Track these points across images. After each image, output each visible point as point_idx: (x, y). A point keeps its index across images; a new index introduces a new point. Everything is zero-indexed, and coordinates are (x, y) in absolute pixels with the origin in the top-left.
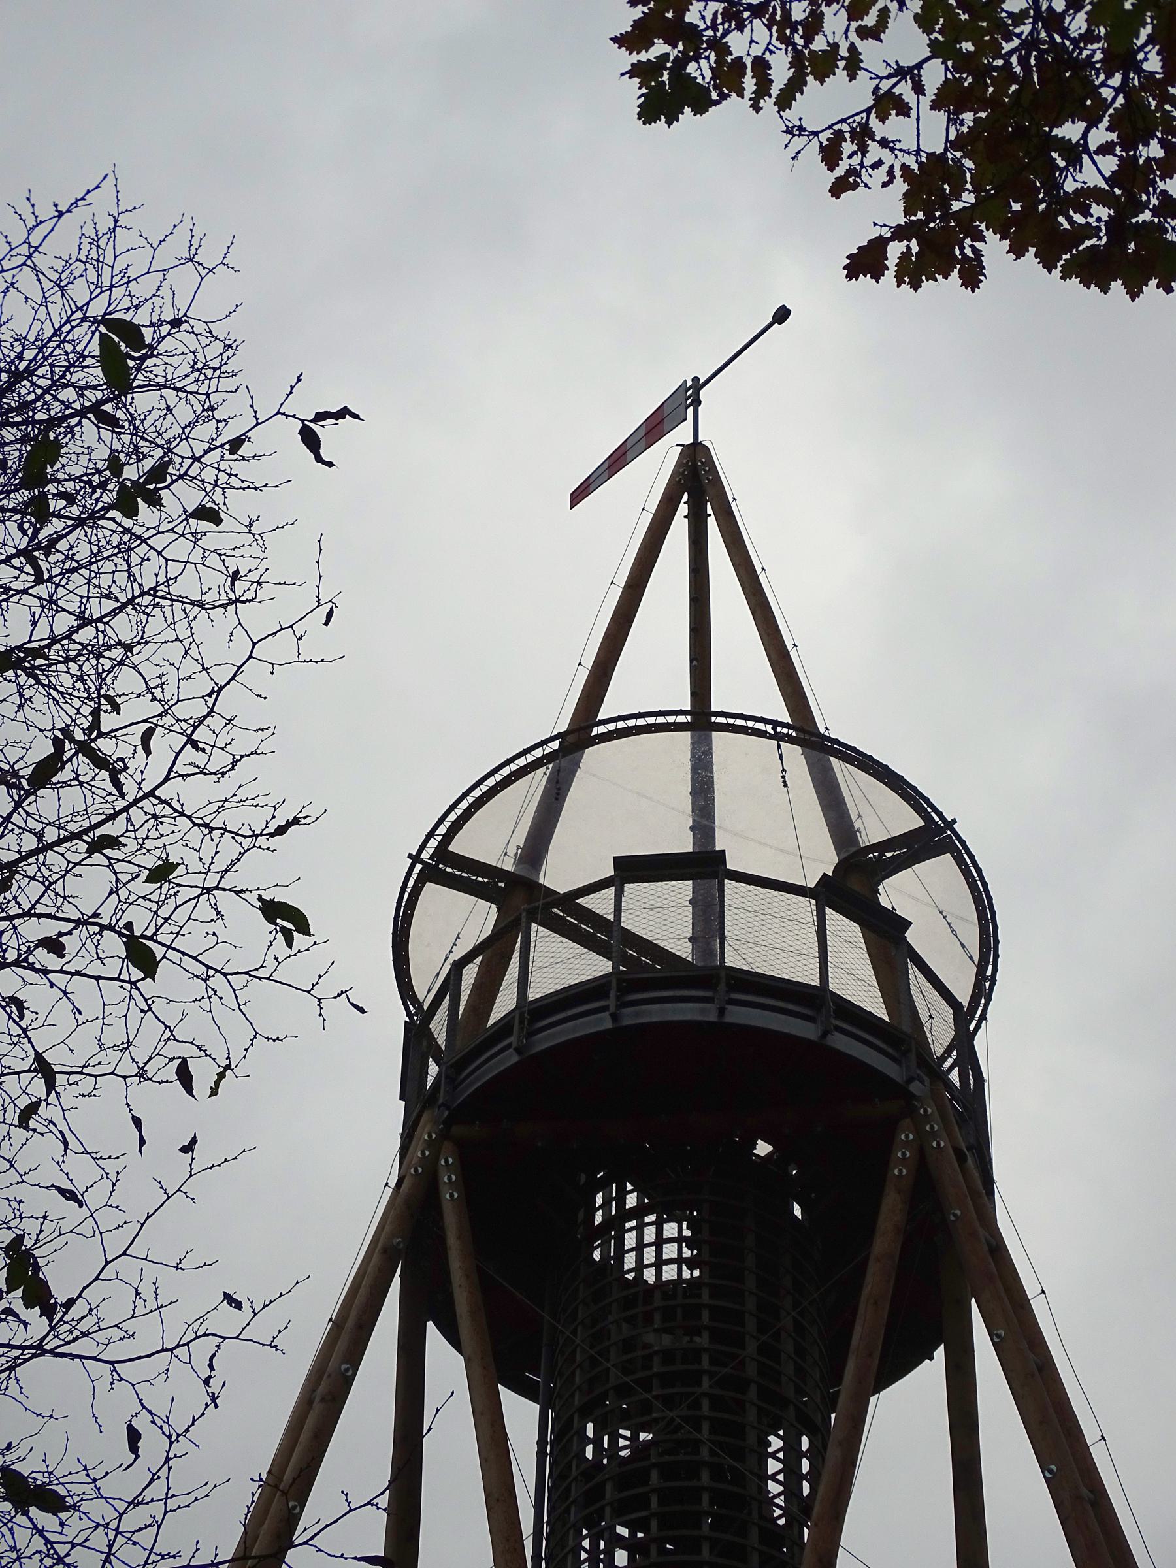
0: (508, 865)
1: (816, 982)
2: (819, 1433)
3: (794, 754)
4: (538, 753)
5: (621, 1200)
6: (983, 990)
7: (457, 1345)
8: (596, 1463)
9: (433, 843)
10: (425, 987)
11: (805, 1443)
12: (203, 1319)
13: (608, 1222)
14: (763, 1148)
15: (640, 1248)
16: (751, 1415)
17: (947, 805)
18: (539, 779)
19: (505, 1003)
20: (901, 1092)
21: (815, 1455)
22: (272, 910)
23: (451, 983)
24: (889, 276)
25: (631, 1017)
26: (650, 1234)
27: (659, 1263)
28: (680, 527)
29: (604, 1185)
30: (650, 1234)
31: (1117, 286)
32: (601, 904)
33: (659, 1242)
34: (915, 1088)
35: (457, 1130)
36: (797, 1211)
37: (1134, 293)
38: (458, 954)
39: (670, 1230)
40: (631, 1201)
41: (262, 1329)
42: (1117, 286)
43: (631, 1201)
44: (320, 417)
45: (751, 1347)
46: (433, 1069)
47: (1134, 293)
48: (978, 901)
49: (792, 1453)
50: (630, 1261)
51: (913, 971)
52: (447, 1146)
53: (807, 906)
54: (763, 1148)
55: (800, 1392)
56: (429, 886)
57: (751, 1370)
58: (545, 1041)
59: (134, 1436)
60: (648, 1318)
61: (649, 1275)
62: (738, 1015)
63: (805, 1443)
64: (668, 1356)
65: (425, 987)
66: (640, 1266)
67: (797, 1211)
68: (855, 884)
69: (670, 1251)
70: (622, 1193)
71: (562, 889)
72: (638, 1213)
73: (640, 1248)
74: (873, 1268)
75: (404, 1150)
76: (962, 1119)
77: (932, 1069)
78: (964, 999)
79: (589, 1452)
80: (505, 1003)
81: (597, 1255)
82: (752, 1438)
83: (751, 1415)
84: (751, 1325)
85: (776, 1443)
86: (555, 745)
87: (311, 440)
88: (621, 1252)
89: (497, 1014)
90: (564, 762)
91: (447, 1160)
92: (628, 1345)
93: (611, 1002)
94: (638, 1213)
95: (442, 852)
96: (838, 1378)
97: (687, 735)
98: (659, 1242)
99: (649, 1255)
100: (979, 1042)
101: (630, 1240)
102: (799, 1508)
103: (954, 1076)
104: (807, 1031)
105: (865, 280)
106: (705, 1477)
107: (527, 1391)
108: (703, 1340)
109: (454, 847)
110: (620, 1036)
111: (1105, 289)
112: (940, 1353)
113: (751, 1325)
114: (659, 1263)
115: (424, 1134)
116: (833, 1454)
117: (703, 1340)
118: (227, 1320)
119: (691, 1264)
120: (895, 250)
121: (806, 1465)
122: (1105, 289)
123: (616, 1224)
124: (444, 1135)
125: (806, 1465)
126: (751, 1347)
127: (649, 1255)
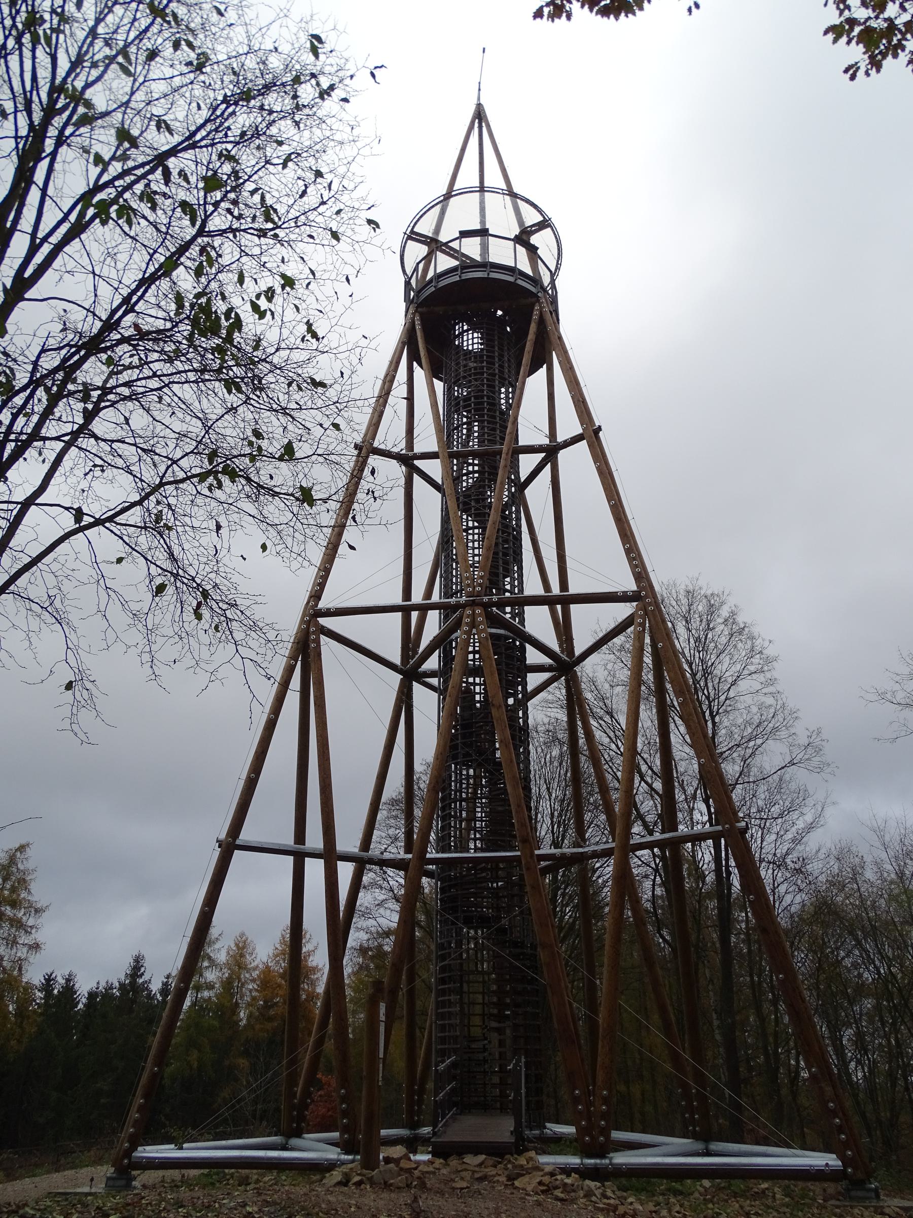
0: (430, 235)
1: (513, 265)
2: (514, 387)
3: (507, 198)
4: (437, 201)
5: (463, 327)
6: (558, 268)
7: (422, 368)
8: (458, 396)
9: (410, 229)
10: (409, 271)
11: (510, 390)
12: (357, 342)
13: (460, 334)
14: (500, 313)
15: (468, 340)
16: (497, 382)
17: (550, 213)
18: (439, 207)
19: (431, 274)
20: (535, 295)
21: (513, 392)
22: (370, 222)
23: (416, 269)
24: (545, 17)
25: (464, 277)
26: (470, 336)
27: (473, 344)
28: (476, 125)
29: (458, 324)
30: (470, 336)
31: (612, 17)
32: (455, 245)
33: (473, 338)
34: (539, 294)
35: (419, 310)
36: (508, 329)
37: (617, 18)
38: (418, 261)
39: (476, 335)
40: (465, 328)
41: (373, 345)
42: (612, 17)
43: (465, 328)
44: (376, 68)
45: (497, 365)
46: (412, 294)
47: (617, 18)
48: (557, 241)
49: (507, 392)
50: (465, 343)
51: (539, 261)
52: (417, 314)
53: (512, 243)
54: (500, 313)
55: (509, 377)
56: (409, 241)
57: (497, 371)
58: (441, 284)
59: (342, 373)
60: (470, 359)
61: (470, 347)
62: (494, 275)
63: (510, 390)
64: (475, 368)
65: (409, 271)
66: (468, 345)
67: (508, 329)
68: (524, 237)
69: (476, 341)
70: (463, 326)
71: (444, 241)
72: (467, 331)
73: (468, 340)
74: (528, 343)
75: (406, 315)
76: (552, 303)
77: (544, 290)
78: (553, 270)
79: (456, 394)
80: (431, 274)
81: (457, 343)
82: (497, 389)
83: (497, 382)
84: (497, 359)
85: (503, 390)
86: (442, 198)
87: (373, 75)
88: (463, 341)
89: (428, 277)
90: (445, 203)
91: (417, 318)
92: (465, 366)
93: (459, 272)
94: (467, 331)
95: (412, 232)
96: (519, 374)
97: (478, 194)
98: (473, 338)
99: (470, 342)
100: (556, 282)
101: (465, 338)
102: (509, 406)
103: (550, 292)
104: (511, 279)
105: (538, 20)
106: (485, 399)
107: (440, 379)
108: (485, 364)
109: (415, 230)
110: (462, 282)
111: (609, 18)
112: (545, 366)
113: (497, 359)
114: (473, 344)
115: (411, 311)
116: (518, 391)
117: (485, 364)
118: (364, 342)
119: (481, 344)
120: (546, 10)
121: (511, 395)
122: (609, 18)
123: (461, 334)
124: (416, 311)
125: (511, 395)
126: (497, 365)
127: (470, 342)
